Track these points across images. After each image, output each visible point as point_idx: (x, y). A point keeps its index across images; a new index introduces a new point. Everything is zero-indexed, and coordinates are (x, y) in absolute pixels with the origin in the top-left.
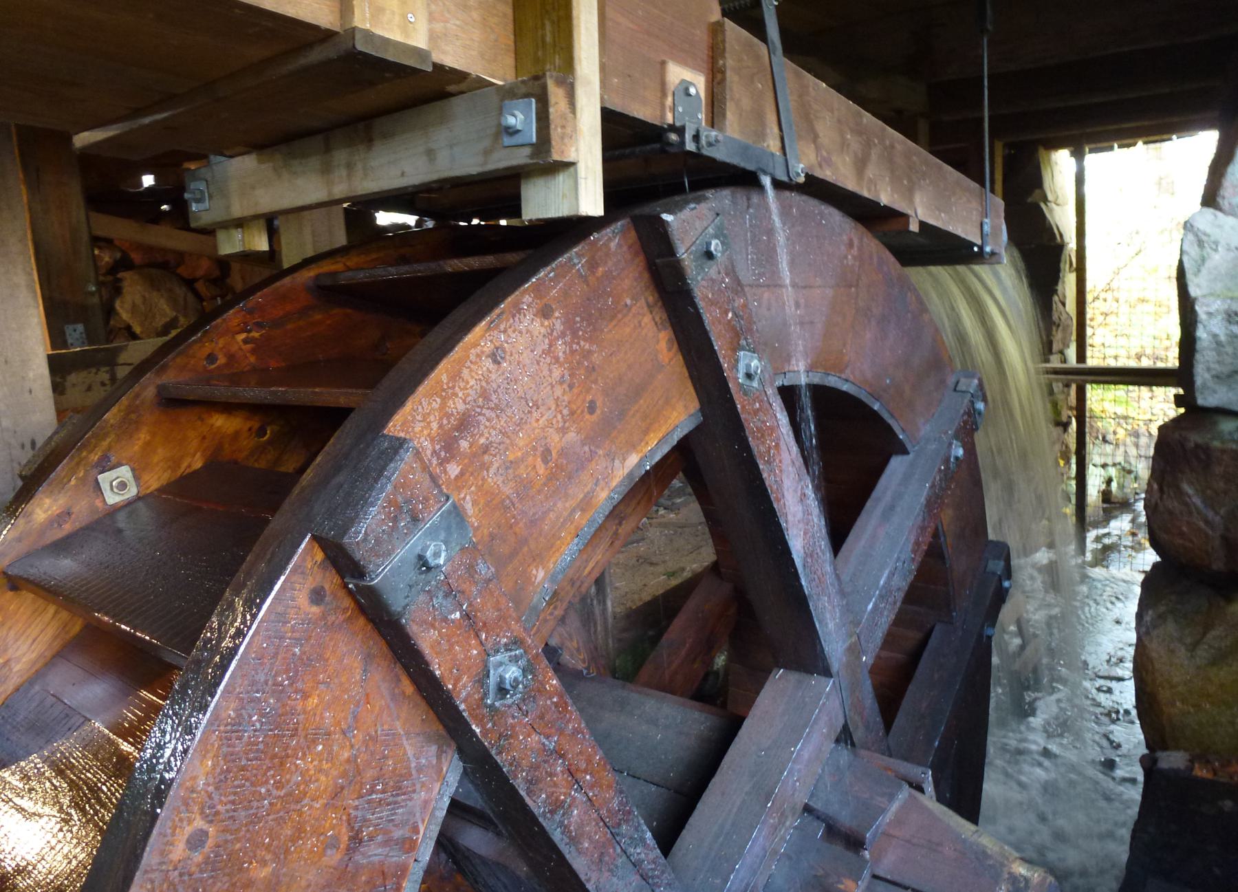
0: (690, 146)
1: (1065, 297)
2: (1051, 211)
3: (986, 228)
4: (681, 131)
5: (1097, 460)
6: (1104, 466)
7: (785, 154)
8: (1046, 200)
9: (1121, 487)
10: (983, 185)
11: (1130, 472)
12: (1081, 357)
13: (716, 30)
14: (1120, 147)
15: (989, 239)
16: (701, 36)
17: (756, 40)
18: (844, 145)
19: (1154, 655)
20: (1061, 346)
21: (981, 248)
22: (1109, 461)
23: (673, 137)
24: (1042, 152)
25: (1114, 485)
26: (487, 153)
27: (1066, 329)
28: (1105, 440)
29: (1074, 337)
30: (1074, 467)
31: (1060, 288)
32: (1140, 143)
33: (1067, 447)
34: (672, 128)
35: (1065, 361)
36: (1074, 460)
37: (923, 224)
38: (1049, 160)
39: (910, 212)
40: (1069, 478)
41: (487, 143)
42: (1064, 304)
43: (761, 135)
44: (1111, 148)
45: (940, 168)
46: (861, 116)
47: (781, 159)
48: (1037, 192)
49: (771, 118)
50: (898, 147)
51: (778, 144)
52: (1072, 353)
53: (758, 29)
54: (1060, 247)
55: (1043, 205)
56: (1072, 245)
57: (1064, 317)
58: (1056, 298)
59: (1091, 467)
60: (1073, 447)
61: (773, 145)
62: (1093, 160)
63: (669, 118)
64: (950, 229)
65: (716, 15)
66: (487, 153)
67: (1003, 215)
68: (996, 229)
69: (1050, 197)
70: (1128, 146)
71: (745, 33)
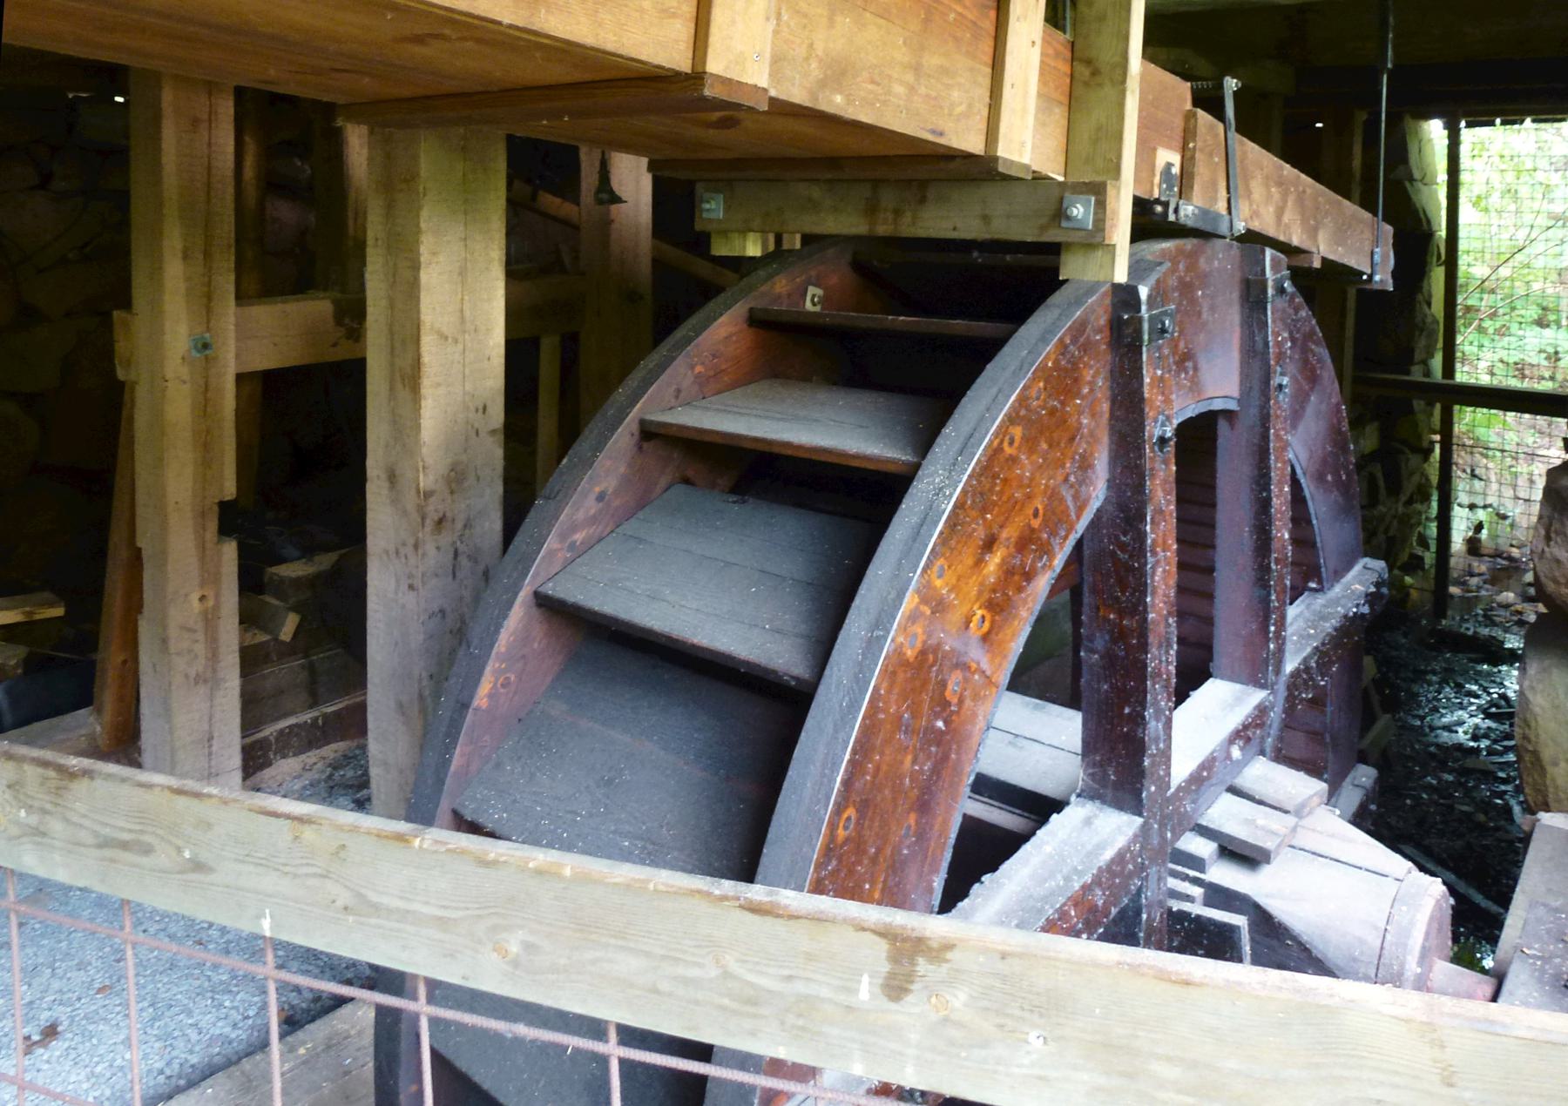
0: (1172, 218)
1: (1430, 296)
2: (1419, 191)
3: (1377, 258)
4: (1166, 205)
5: (1463, 498)
6: (1472, 507)
7: (1230, 213)
8: (1411, 179)
9: (1493, 536)
10: (1375, 214)
11: (1504, 517)
12: (1449, 370)
13: (1189, 117)
14: (1503, 123)
15: (1378, 268)
16: (1179, 123)
17: (1215, 121)
18: (1269, 197)
19: (1537, 710)
20: (1423, 356)
21: (1371, 277)
22: (1479, 501)
23: (1159, 209)
24: (1409, 122)
25: (1484, 534)
26: (1043, 228)
27: (1432, 335)
28: (1474, 476)
29: (1440, 344)
30: (1435, 505)
31: (1425, 284)
32: (1528, 120)
33: (1428, 480)
34: (1157, 201)
35: (1428, 373)
36: (1435, 497)
37: (1324, 259)
38: (1417, 132)
39: (1314, 250)
40: (1427, 519)
41: (1044, 221)
42: (1429, 304)
43: (1215, 200)
44: (1492, 124)
45: (1340, 204)
46: (1282, 168)
47: (1227, 218)
48: (1401, 168)
49: (1223, 184)
50: (1309, 191)
51: (1225, 205)
52: (1437, 362)
53: (1219, 114)
54: (1429, 235)
55: (1407, 184)
56: (1443, 233)
57: (1429, 320)
58: (1420, 297)
59: (1456, 508)
60: (1435, 479)
61: (1221, 207)
62: (1468, 135)
63: (1156, 195)
64: (1345, 261)
65: (1188, 106)
66: (1043, 228)
67: (1391, 241)
68: (1385, 257)
69: (1417, 175)
70: (1513, 123)
71: (1210, 117)
